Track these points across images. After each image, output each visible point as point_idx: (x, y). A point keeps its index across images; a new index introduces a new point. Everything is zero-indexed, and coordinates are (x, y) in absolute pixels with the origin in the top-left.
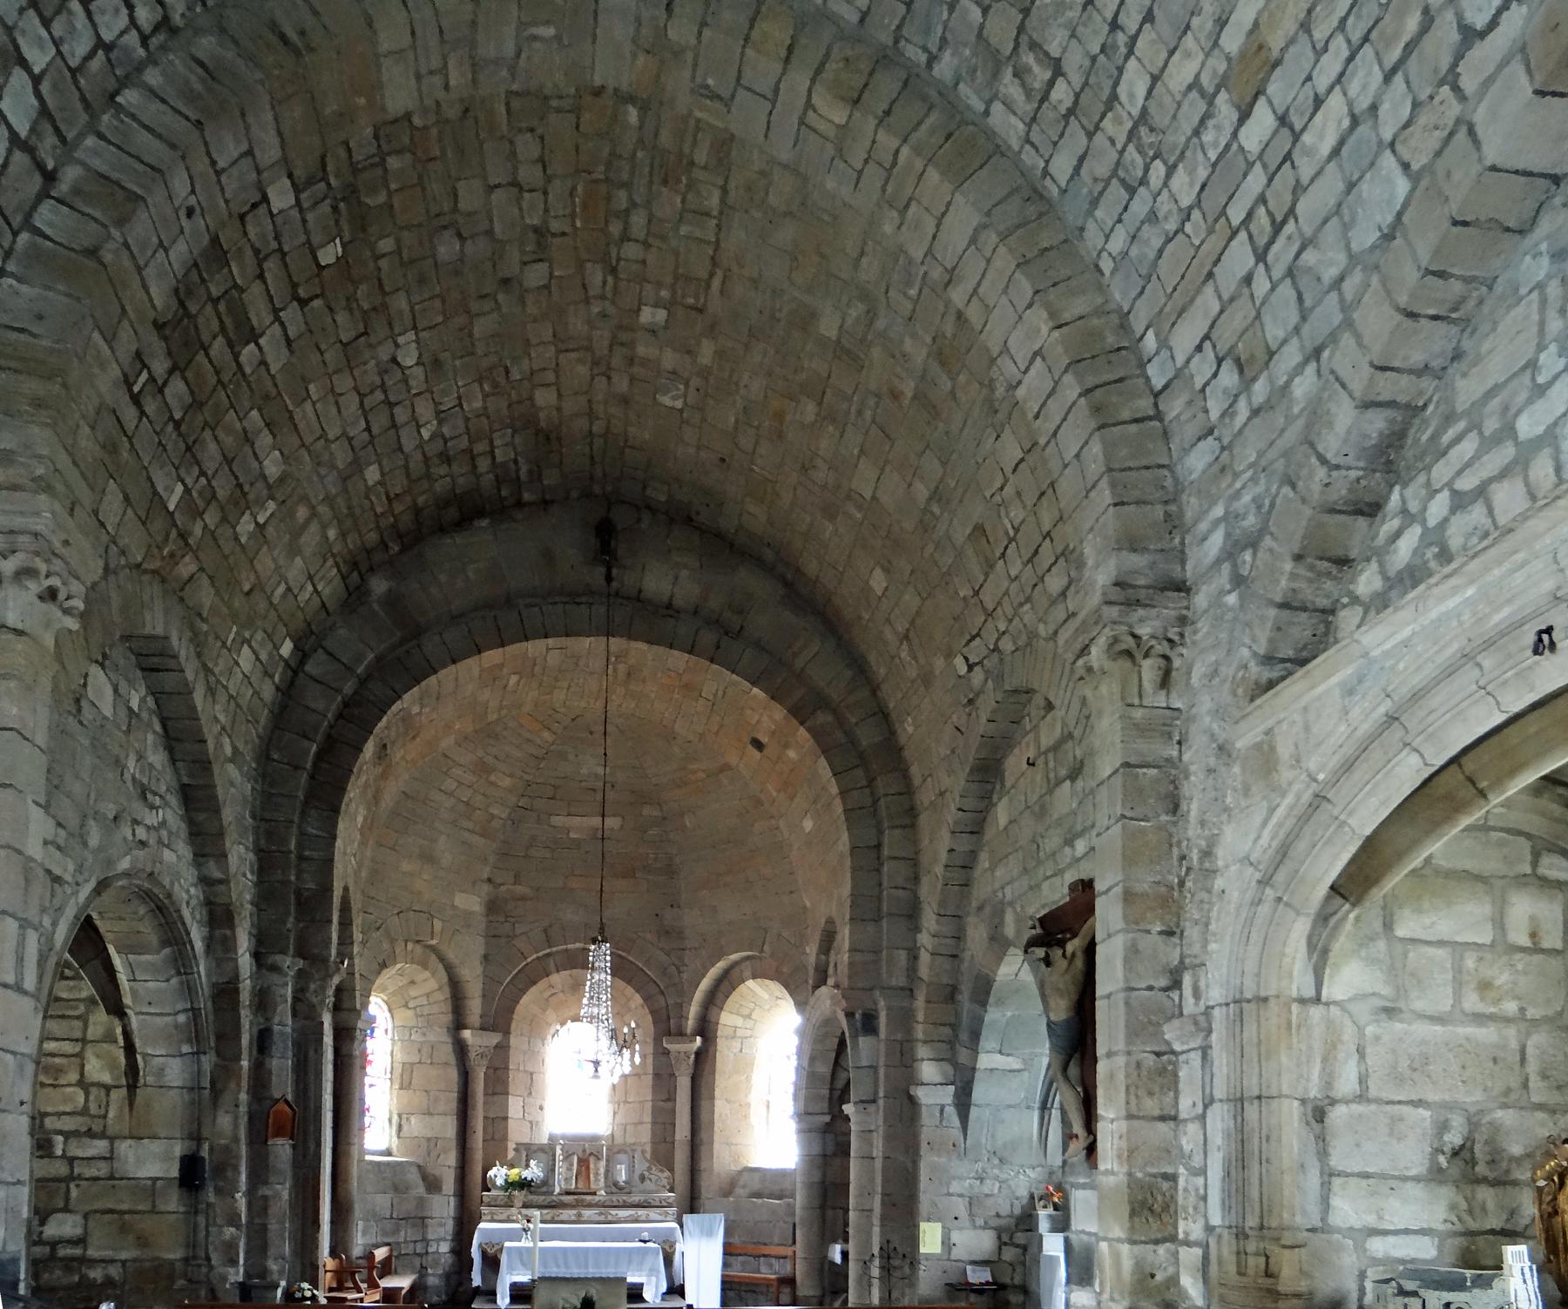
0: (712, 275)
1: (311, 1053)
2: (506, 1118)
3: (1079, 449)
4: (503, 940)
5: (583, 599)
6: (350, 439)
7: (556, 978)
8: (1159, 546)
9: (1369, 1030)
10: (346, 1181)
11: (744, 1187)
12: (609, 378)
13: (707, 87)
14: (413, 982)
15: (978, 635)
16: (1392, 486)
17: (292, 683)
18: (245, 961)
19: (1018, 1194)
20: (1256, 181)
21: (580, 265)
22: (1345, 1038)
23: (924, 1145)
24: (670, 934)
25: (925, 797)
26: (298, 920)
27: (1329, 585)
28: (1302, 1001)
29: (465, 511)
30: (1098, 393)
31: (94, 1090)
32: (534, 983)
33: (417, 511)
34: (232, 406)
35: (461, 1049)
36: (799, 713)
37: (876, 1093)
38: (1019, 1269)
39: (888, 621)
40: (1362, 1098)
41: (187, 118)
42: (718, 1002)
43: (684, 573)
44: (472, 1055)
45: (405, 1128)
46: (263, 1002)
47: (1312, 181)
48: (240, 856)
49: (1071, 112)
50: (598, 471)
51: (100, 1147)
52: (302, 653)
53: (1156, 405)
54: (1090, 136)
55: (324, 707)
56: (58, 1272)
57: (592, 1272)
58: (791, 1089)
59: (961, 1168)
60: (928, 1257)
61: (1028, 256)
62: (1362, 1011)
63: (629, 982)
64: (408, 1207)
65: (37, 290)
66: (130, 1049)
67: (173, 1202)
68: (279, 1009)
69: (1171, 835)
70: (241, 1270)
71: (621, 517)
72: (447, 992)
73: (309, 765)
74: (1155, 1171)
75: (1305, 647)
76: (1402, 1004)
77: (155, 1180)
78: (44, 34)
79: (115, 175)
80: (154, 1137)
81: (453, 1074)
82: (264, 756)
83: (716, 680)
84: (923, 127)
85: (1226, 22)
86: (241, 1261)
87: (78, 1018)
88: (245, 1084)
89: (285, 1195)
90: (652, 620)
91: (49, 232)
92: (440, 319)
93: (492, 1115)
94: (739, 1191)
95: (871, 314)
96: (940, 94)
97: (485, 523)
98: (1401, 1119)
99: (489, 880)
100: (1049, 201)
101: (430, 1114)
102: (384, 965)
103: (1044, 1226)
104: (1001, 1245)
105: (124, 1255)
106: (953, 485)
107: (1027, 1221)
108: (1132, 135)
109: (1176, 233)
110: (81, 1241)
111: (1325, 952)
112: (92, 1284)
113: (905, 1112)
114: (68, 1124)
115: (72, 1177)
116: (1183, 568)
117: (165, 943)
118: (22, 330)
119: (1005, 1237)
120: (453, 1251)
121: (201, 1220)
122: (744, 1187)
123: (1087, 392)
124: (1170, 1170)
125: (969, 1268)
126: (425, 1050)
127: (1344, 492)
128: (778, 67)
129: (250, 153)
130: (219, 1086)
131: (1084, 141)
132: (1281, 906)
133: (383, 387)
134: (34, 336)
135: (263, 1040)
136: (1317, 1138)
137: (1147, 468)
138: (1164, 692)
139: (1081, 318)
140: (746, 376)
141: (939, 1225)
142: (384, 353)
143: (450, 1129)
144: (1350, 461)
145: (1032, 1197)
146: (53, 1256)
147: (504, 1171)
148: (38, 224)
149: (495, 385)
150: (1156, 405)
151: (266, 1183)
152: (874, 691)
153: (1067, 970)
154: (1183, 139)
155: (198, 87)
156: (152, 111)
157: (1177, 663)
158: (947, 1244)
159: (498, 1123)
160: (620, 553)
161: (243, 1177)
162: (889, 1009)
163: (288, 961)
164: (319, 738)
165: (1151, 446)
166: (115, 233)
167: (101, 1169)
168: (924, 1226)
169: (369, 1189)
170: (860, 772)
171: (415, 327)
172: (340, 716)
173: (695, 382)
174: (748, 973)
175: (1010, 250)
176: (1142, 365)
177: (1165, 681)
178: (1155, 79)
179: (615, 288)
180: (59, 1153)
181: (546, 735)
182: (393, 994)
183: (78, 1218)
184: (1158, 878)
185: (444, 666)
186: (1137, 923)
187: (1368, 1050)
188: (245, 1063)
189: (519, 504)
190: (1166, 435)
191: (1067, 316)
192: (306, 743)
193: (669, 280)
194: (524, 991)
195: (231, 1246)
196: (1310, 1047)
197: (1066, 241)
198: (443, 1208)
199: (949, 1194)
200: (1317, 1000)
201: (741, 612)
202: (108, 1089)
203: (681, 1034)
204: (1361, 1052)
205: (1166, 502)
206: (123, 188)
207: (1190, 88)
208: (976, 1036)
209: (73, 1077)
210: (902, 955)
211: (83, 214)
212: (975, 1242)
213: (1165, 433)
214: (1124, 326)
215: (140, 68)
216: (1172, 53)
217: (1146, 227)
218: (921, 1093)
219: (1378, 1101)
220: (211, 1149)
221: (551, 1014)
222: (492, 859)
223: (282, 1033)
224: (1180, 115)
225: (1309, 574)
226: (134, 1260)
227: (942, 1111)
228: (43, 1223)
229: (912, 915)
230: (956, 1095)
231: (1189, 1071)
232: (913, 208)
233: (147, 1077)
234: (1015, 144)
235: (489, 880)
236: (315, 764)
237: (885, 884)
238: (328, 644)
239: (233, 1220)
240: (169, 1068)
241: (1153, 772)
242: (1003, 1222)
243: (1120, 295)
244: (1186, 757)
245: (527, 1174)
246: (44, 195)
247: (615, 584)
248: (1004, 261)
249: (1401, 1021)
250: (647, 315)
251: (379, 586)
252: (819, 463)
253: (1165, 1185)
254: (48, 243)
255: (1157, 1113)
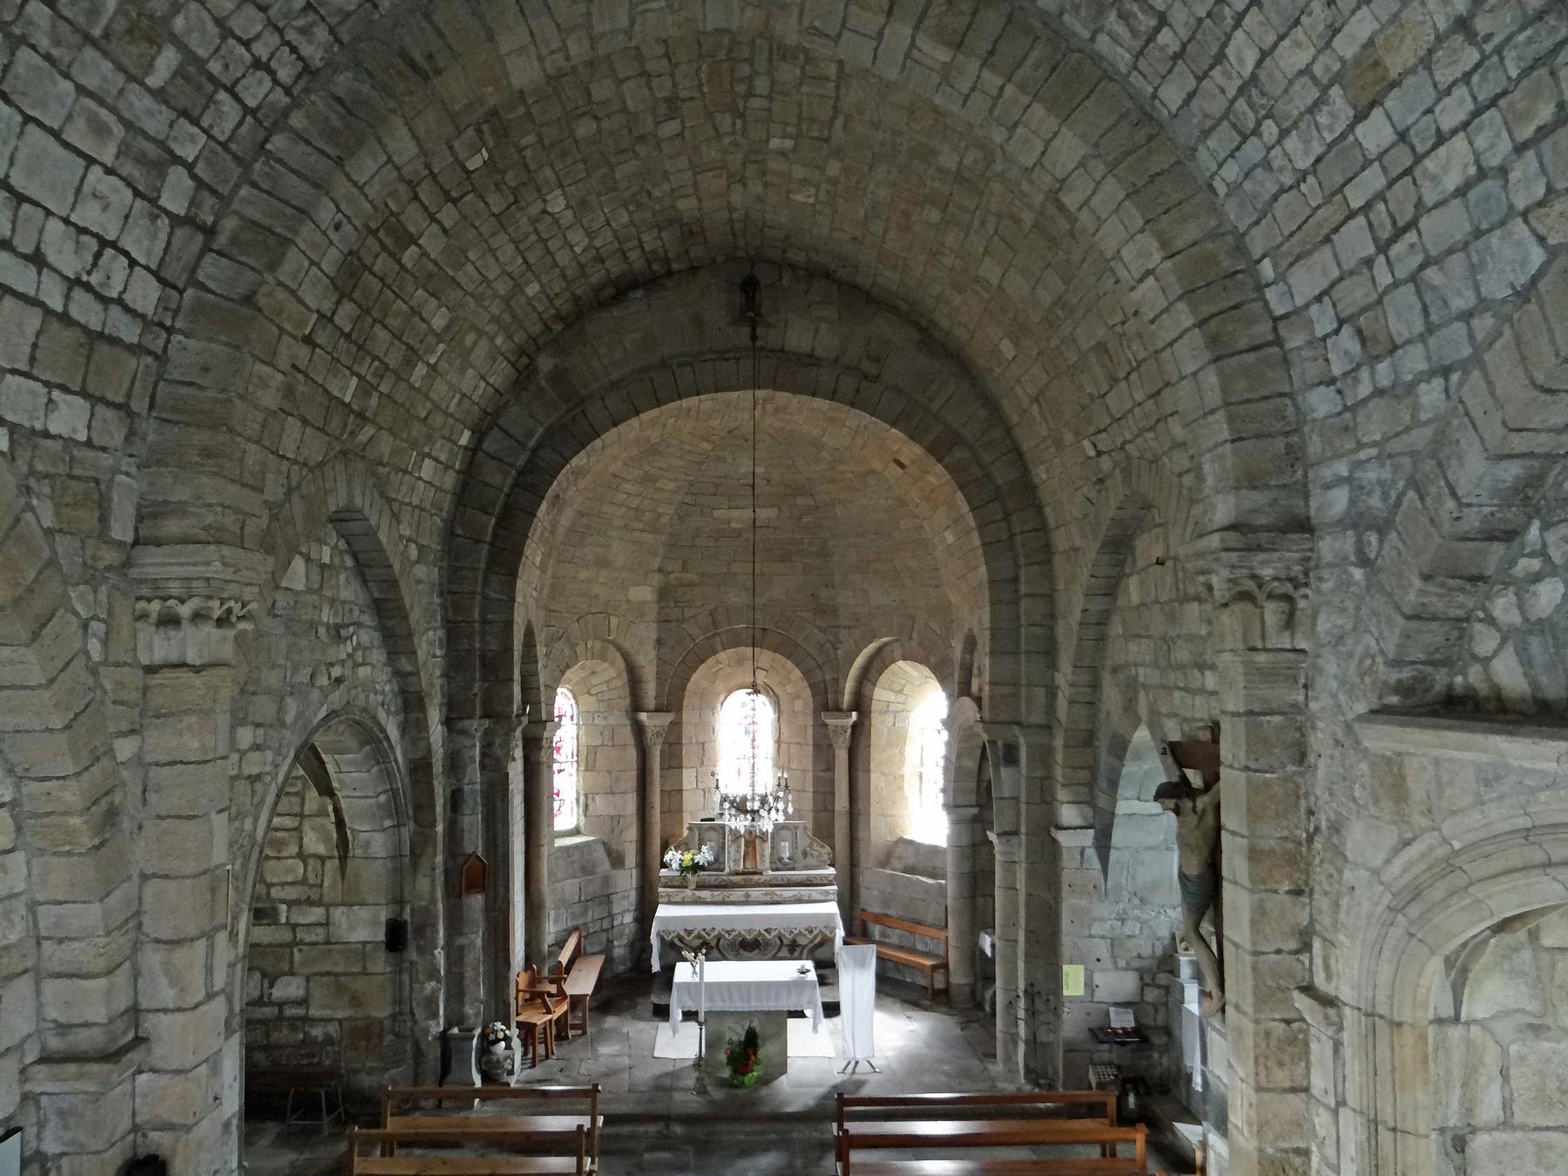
0: (834, 118)
1: (499, 803)
2: (681, 791)
3: (1195, 379)
4: (673, 625)
5: (730, 355)
6: (509, 275)
7: (723, 656)
8: (1282, 481)
9: (1513, 1049)
10: (538, 881)
11: (900, 858)
12: (745, 185)
13: (814, 28)
14: (594, 673)
15: (1105, 430)
16: (1531, 518)
17: (471, 463)
18: (436, 732)
19: (1159, 934)
20: (1373, 179)
21: (710, 116)
22: (1487, 1059)
23: (1065, 889)
24: (826, 610)
25: (1060, 541)
26: (484, 680)
27: (1461, 598)
28: (1439, 1021)
29: (620, 291)
30: (1213, 323)
31: (311, 862)
32: (703, 661)
33: (576, 299)
34: (398, 296)
35: (639, 730)
36: (937, 450)
37: (1018, 824)
38: (1162, 1012)
39: (1018, 381)
40: (1506, 1124)
41: (329, 157)
42: (871, 676)
43: (824, 327)
44: (649, 734)
45: (591, 808)
46: (454, 763)
47: (1435, 207)
48: (429, 646)
49: (1177, 57)
50: (741, 243)
51: (316, 914)
52: (479, 434)
53: (1275, 329)
54: (1199, 79)
55: (498, 479)
56: (285, 1031)
57: (755, 1005)
58: (942, 763)
59: (1104, 909)
60: (1072, 999)
61: (1139, 184)
62: (1506, 1029)
63: (788, 657)
64: (595, 888)
65: (203, 344)
66: (340, 824)
67: (381, 964)
68: (469, 770)
69: (1298, 787)
70: (442, 1021)
71: (765, 276)
72: (625, 678)
73: (488, 538)
74: (1285, 1145)
75: (1437, 650)
76: (1549, 1021)
77: (365, 943)
78: (195, 130)
79: (267, 222)
80: (363, 904)
81: (632, 753)
82: (449, 534)
83: (857, 418)
84: (1029, 62)
85: (1339, 30)
86: (441, 1012)
87: (296, 794)
88: (440, 846)
89: (479, 942)
90: (794, 372)
91: (211, 284)
92: (583, 175)
93: (667, 788)
94: (895, 863)
95: (989, 160)
96: (1045, 24)
97: (639, 293)
98: (1550, 1147)
99: (660, 570)
100: (1161, 126)
101: (612, 793)
102: (568, 667)
103: (1185, 971)
104: (1144, 986)
105: (340, 1015)
106: (1075, 301)
107: (1168, 963)
108: (1242, 90)
109: (1291, 188)
110: (303, 1002)
111: (1465, 971)
112: (314, 1041)
113: (1046, 857)
114: (291, 893)
115: (294, 943)
116: (1307, 505)
117: (362, 744)
118: (191, 384)
119: (1147, 978)
120: (636, 920)
121: (406, 978)
122: (900, 858)
123: (1201, 324)
124: (1302, 1145)
125: (1112, 1009)
126: (606, 733)
127: (1477, 524)
128: (882, 20)
129: (390, 160)
130: (418, 852)
131: (1194, 82)
132: (1414, 941)
133: (536, 232)
134: (200, 387)
135: (455, 801)
136: (1457, 1169)
137: (1266, 398)
138: (1287, 634)
139: (1195, 243)
140: (872, 187)
141: (1081, 968)
142: (535, 209)
143: (630, 805)
144: (1483, 500)
145: (1173, 937)
146: (280, 1017)
147: (678, 855)
148: (201, 278)
149: (639, 205)
150: (1275, 329)
151: (461, 934)
152: (1009, 431)
153: (1197, 826)
154: (1296, 112)
155: (338, 124)
156: (298, 154)
157: (1302, 604)
158: (1090, 986)
159: (674, 796)
160: (763, 310)
161: (441, 933)
162: (1029, 747)
163: (475, 723)
164: (497, 510)
165: (1270, 374)
166: (269, 278)
167: (318, 935)
168: (1067, 968)
169: (560, 875)
170: (995, 506)
171: (561, 186)
172: (516, 484)
173: (824, 187)
174: (898, 654)
175: (1120, 180)
176: (1260, 287)
177: (1289, 623)
178: (1264, 55)
179: (744, 126)
180: (283, 920)
181: (706, 446)
182: (577, 683)
183: (301, 981)
184: (1286, 833)
185: (607, 430)
186: (1264, 882)
187: (1513, 1072)
188: (440, 828)
189: (670, 273)
190: (1286, 362)
191: (1179, 244)
192: (485, 518)
193: (794, 121)
194: (694, 669)
195: (431, 1002)
196: (1448, 1071)
197: (1178, 162)
198: (627, 881)
199: (1091, 936)
200: (1457, 1019)
201: (878, 360)
202: (322, 859)
203: (837, 709)
204: (1504, 1074)
205: (1287, 434)
206: (273, 233)
207: (1301, 73)
208: (1114, 785)
209: (293, 849)
210: (1040, 693)
211: (240, 262)
212: (1118, 983)
213: (1285, 359)
214: (1240, 248)
215: (286, 112)
216: (1282, 38)
217: (1259, 171)
218: (1063, 838)
219: (1523, 1127)
220: (412, 910)
221: (719, 686)
222: (661, 550)
223: (472, 792)
224: (1291, 91)
225: (1439, 590)
226: (349, 1019)
227: (1082, 853)
228: (271, 986)
229: (1049, 652)
230: (1096, 838)
231: (1320, 1049)
232: (1020, 130)
233: (356, 851)
234: (1123, 69)
235: (660, 570)
236: (495, 534)
237: (1023, 621)
238: (501, 422)
239: (433, 974)
240: (374, 842)
241: (1277, 719)
242: (1146, 963)
243: (1237, 216)
244: (1313, 705)
245: (700, 859)
246: (206, 249)
247: (759, 343)
248: (1112, 189)
249: (1549, 1040)
250: (775, 143)
251: (546, 363)
252: (947, 251)
253: (1298, 1161)
254: (211, 296)
255: (1287, 1084)
